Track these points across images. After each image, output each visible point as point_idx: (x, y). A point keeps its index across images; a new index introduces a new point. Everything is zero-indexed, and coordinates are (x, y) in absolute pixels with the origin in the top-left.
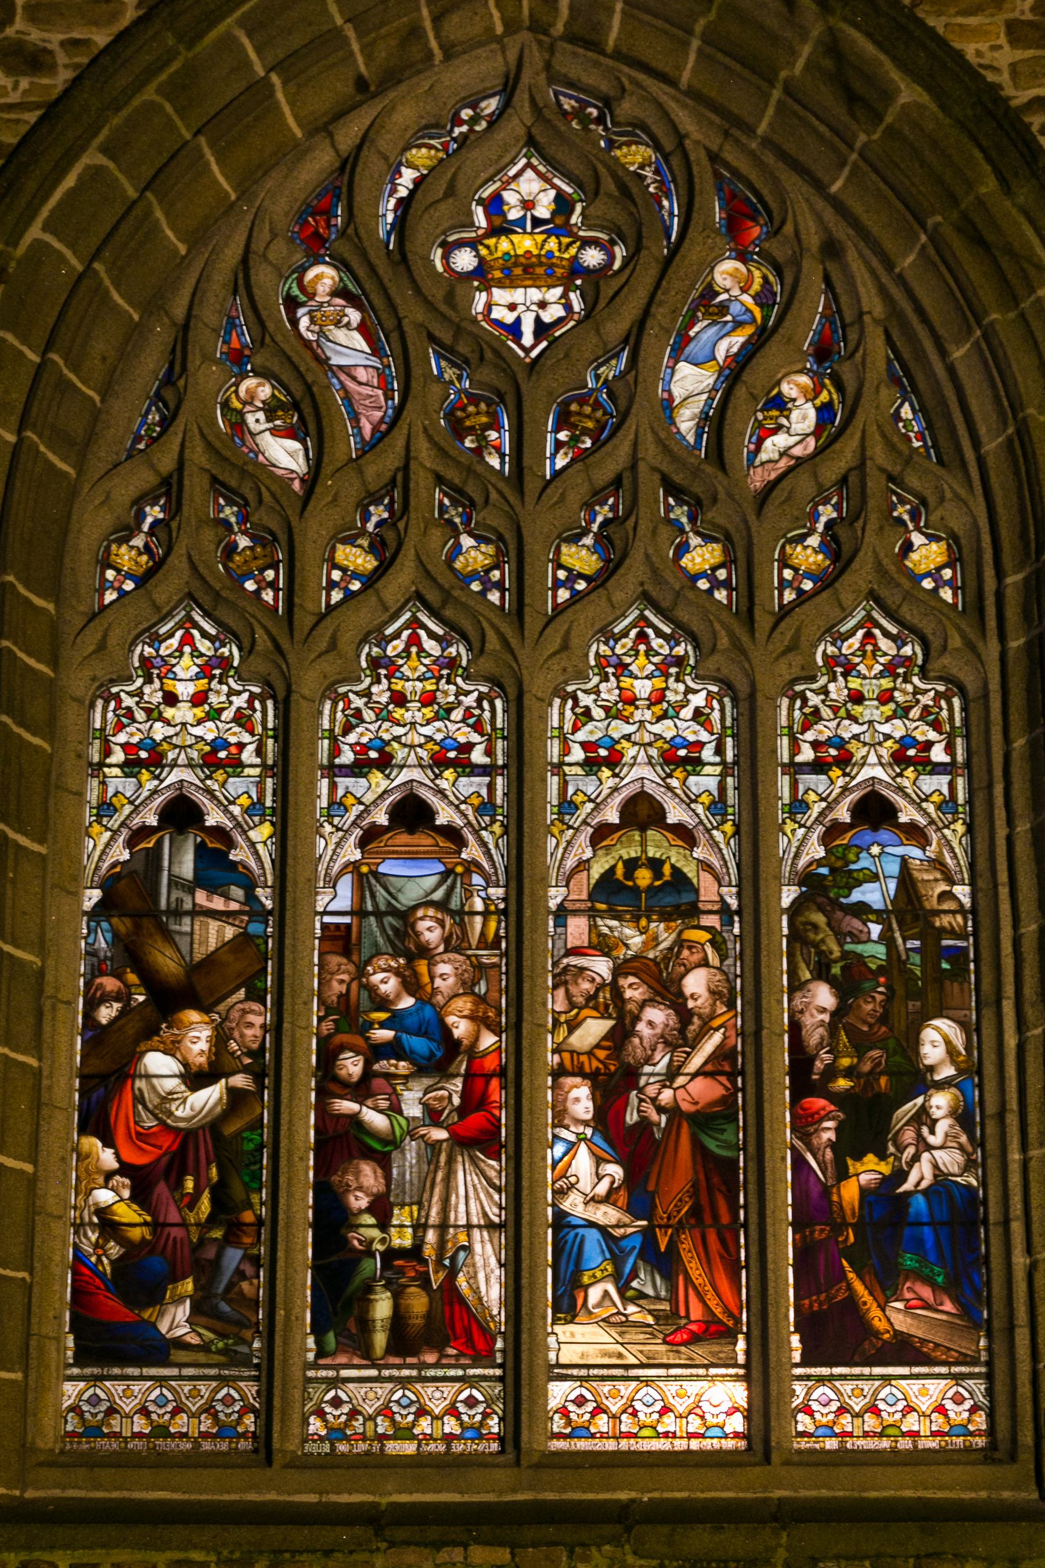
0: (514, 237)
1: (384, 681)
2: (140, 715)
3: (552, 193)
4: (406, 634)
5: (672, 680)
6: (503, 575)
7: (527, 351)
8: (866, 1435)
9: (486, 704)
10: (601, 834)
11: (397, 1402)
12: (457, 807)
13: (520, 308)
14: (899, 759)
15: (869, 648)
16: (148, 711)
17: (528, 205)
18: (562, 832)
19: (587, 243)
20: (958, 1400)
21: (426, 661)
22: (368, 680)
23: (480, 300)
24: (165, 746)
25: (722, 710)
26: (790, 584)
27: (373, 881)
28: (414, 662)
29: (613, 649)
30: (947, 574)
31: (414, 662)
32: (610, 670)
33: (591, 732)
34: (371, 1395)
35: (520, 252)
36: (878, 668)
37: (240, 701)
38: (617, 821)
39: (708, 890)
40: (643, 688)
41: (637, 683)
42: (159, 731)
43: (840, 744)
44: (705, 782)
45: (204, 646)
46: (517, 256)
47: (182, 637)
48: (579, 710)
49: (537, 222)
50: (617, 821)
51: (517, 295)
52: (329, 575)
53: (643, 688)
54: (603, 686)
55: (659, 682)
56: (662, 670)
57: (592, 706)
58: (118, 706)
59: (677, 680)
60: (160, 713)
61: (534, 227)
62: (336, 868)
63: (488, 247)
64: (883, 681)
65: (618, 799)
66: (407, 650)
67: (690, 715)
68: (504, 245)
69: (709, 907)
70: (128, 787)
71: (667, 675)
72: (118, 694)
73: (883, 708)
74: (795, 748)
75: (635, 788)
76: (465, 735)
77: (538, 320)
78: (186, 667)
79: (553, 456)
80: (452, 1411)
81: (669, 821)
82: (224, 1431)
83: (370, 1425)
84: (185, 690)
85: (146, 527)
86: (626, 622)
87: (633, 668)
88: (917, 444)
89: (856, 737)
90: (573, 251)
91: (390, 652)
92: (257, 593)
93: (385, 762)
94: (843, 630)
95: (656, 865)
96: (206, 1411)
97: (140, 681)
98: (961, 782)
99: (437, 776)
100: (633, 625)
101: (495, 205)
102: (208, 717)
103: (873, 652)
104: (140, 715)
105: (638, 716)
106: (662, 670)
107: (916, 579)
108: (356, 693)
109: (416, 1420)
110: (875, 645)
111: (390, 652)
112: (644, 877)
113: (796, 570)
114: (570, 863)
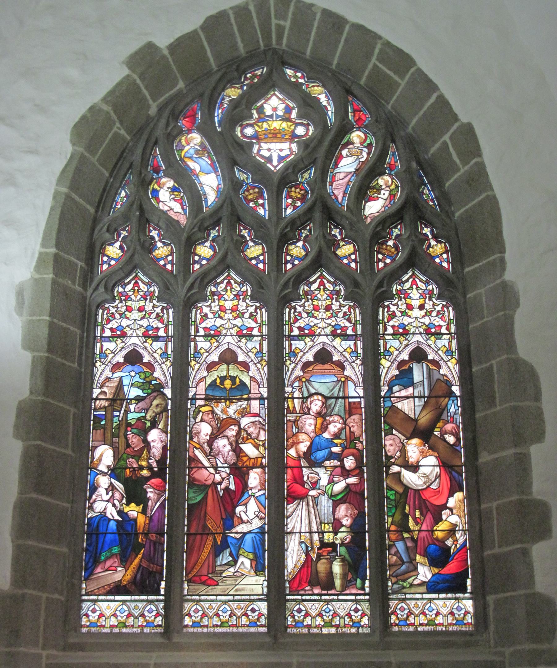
0: (269, 122)
1: (124, 302)
2: (117, 316)
3: (284, 106)
4: (226, 281)
5: (334, 301)
6: (173, 258)
7: (275, 167)
8: (214, 626)
9: (165, 311)
10: (211, 367)
11: (324, 611)
12: (437, 352)
13: (272, 151)
14: (145, 335)
15: (136, 288)
16: (121, 315)
17: (275, 109)
18: (290, 364)
19: (297, 124)
20: (356, 610)
21: (327, 292)
22: (210, 301)
23: (256, 148)
24: (222, 328)
25: (262, 315)
26: (106, 262)
27: (308, 384)
28: (322, 292)
29: (217, 289)
30: (445, 256)
31: (322, 292)
32: (402, 296)
33: (249, 323)
34: (342, 607)
35: (272, 128)
36: (139, 297)
37: (345, 309)
38: (312, 360)
39: (254, 388)
40: (228, 305)
41: (320, 303)
42: (406, 320)
43: (121, 328)
44: (444, 342)
45: (236, 287)
46: (270, 130)
47: (134, 284)
48: (202, 314)
49: (278, 116)
50: (312, 360)
51: (272, 146)
52: (193, 258)
53: (228, 305)
54: (306, 304)
55: (235, 302)
56: (144, 298)
57: (396, 311)
58: (295, 311)
59: (336, 301)
60: (125, 315)
61: (277, 118)
62: (293, 377)
63: (258, 126)
64: (234, 302)
65: (124, 352)
66: (319, 288)
67: (155, 316)
68: (265, 125)
69: (201, 397)
70: (207, 345)
71: (146, 300)
72: (295, 306)
73: (233, 314)
74: (103, 331)
75: (226, 346)
76: (156, 324)
77: (279, 156)
78: (229, 295)
79: (286, 209)
80: (320, 615)
81: (239, 360)
82: (149, 624)
83: (342, 620)
84: (416, 303)
85: (210, 239)
86: (131, 277)
87: (225, 296)
88: (431, 203)
89: (128, 326)
90: (293, 127)
91: (219, 289)
92: (165, 265)
93: (312, 334)
94: (311, 280)
95: (233, 379)
96: (318, 615)
97: (397, 300)
98: (359, 344)
99: (428, 339)
100: (411, 277)
101: (261, 110)
102: (238, 316)
103: (138, 290)
104: (117, 316)
105: (226, 316)
106: (237, 296)
107: (433, 258)
108: (299, 306)
109: (332, 618)
110: (139, 287)
111: (219, 289)
112: (228, 384)
113: (292, 256)
114: (198, 377)
